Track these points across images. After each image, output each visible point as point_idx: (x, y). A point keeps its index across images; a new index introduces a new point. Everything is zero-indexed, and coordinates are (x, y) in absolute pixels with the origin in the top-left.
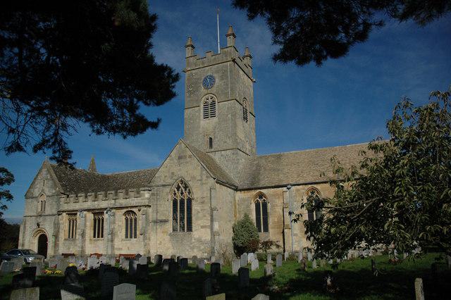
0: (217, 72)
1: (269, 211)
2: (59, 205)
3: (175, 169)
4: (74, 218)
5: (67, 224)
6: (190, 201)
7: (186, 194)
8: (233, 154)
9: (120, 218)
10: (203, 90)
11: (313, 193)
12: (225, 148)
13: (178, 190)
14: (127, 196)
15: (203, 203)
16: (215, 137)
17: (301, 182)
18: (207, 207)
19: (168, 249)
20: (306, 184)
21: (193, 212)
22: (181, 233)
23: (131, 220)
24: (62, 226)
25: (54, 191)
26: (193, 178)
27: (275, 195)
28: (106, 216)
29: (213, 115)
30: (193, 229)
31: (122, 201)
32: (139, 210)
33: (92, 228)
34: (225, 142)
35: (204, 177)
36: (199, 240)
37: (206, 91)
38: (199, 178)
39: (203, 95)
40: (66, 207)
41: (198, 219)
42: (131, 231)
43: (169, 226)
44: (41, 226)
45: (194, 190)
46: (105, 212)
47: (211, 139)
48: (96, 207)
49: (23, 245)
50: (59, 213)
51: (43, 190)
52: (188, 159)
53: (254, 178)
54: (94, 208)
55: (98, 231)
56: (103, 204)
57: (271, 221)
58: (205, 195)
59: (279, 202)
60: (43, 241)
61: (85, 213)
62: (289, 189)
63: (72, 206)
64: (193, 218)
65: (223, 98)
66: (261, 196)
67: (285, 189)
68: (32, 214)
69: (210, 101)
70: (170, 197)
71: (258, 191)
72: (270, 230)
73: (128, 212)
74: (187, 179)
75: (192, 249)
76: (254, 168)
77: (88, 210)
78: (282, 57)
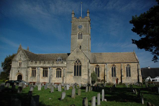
0: (83, 24)
1: (100, 70)
2: (28, 64)
3: (75, 55)
4: (35, 70)
5: (31, 72)
6: (80, 66)
7: (79, 64)
8: (88, 52)
9: (54, 71)
10: (78, 29)
11: (113, 66)
12: (85, 50)
13: (76, 62)
14: (44, 63)
15: (85, 67)
16: (82, 46)
17: (110, 62)
18: (87, 68)
19: (72, 81)
20: (111, 63)
21: (82, 70)
22: (77, 76)
23: (45, 71)
24: (29, 72)
25: (25, 59)
26: (82, 59)
27: (102, 66)
28: (49, 70)
29: (82, 38)
30: (82, 75)
31: (55, 65)
32: (62, 68)
33: (42, 73)
34: (86, 48)
35: (86, 59)
36: (84, 79)
37: (79, 30)
38: (84, 59)
39: (78, 31)
40: (31, 65)
41: (83, 72)
42: (59, 74)
43: (73, 74)
44: (19, 72)
45: (82, 63)
46: (48, 68)
47: (80, 46)
48: (45, 66)
49: (11, 78)
50: (28, 67)
51: (20, 59)
52: (80, 53)
53: (94, 60)
54: (43, 66)
55: (45, 74)
56: (48, 65)
57: (100, 74)
58: (86, 64)
59: (103, 68)
60: (20, 77)
61: (39, 68)
62: (106, 64)
63: (34, 65)
64: (82, 72)
65: (85, 33)
66: (97, 66)
67: (105, 64)
68: (15, 67)
69: (80, 33)
70: (73, 64)
71: (97, 64)
72: (100, 76)
73: (58, 69)
74: (80, 59)
75: (81, 81)
76: (93, 57)
77: (41, 67)
78: (132, 30)
